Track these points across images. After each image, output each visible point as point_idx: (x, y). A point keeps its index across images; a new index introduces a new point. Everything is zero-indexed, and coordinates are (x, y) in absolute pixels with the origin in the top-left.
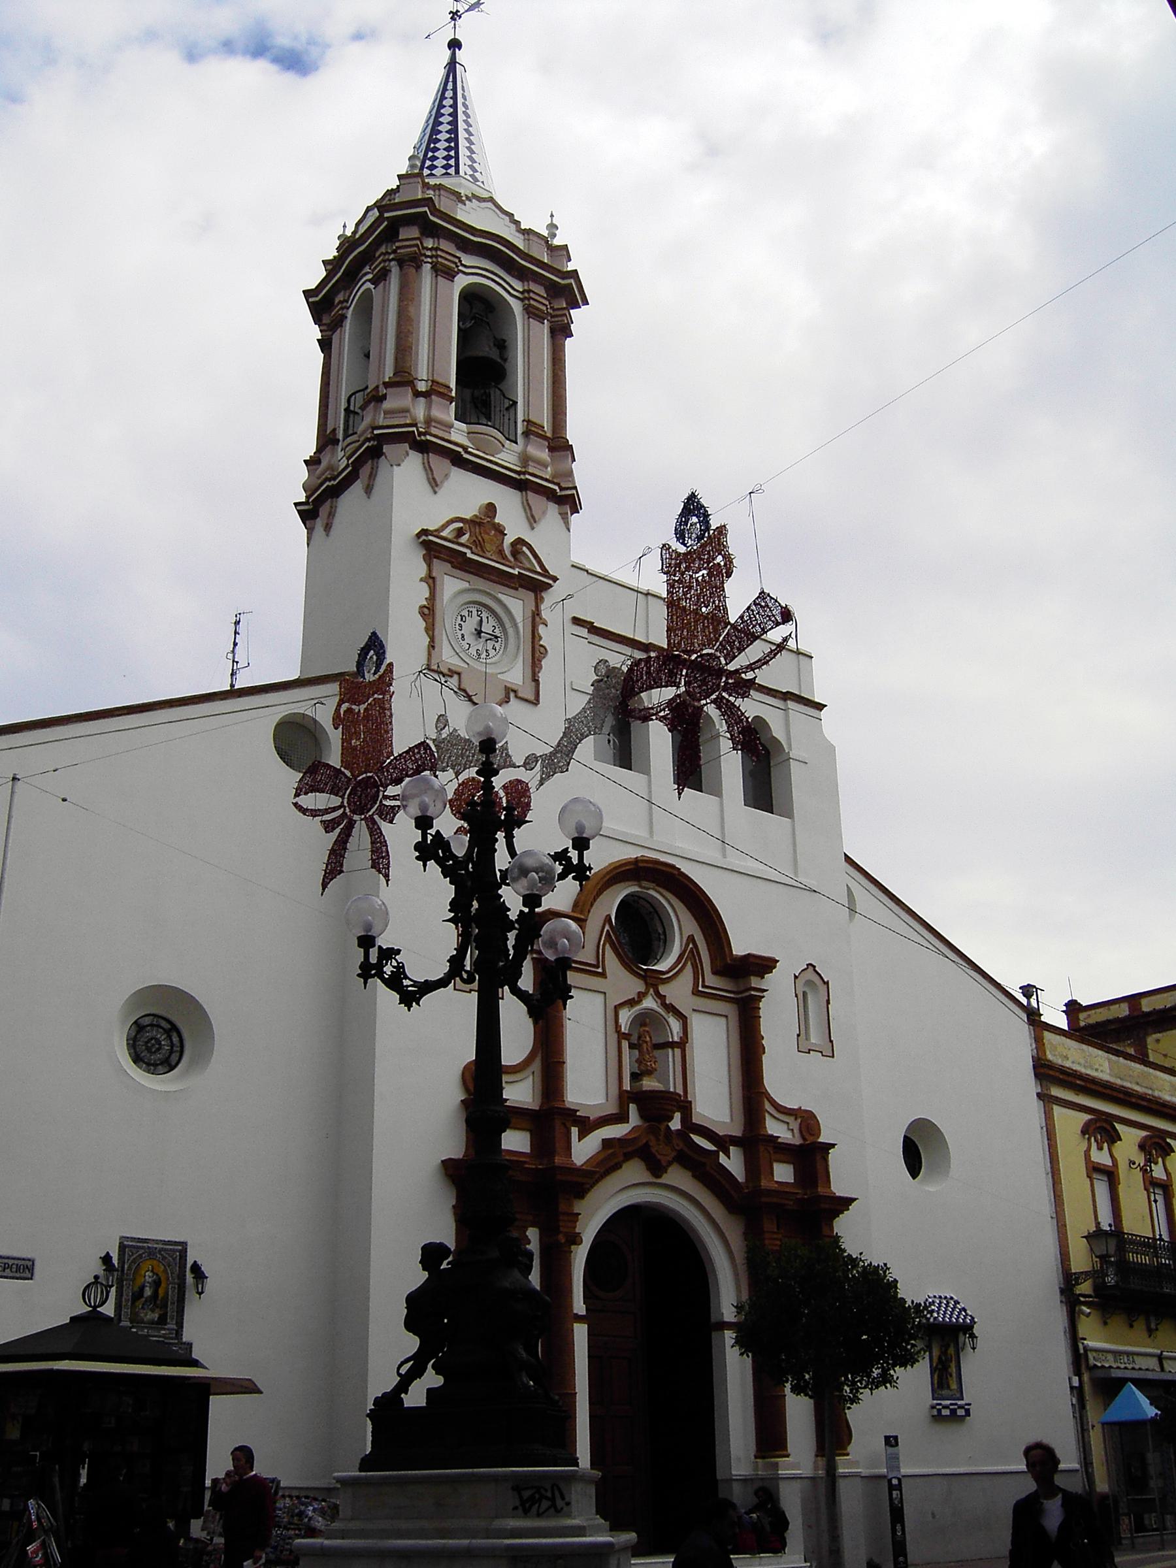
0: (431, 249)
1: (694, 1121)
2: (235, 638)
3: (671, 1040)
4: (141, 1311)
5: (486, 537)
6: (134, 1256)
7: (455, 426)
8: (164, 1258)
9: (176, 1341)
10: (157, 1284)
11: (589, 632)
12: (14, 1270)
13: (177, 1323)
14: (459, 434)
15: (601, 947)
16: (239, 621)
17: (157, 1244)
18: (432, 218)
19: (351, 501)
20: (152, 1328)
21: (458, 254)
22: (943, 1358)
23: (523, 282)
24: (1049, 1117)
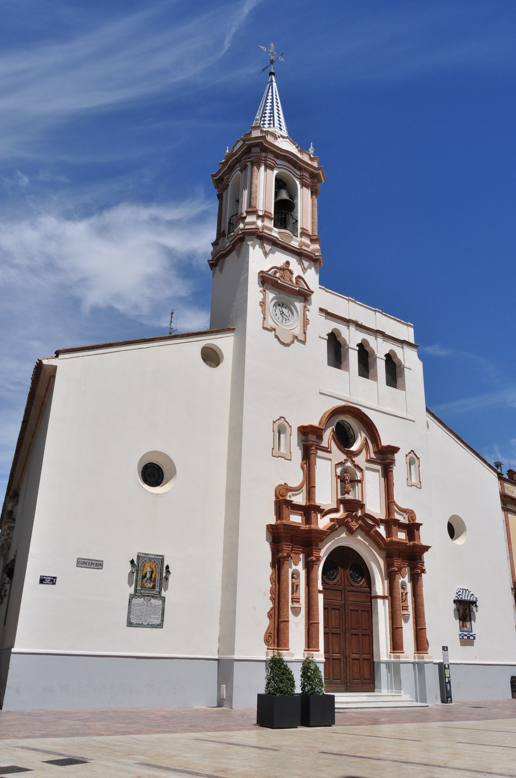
0: (264, 157)
1: (366, 512)
2: (171, 319)
3: (357, 479)
4: (146, 583)
5: (286, 275)
6: (143, 561)
7: (274, 230)
8: (155, 562)
9: (159, 596)
10: (152, 572)
12: (95, 565)
13: (159, 589)
14: (275, 233)
15: (330, 440)
16: (173, 313)
17: (152, 556)
18: (265, 144)
19: (231, 259)
20: (149, 590)
21: (275, 159)
22: (464, 615)
23: (300, 171)
24: (506, 518)
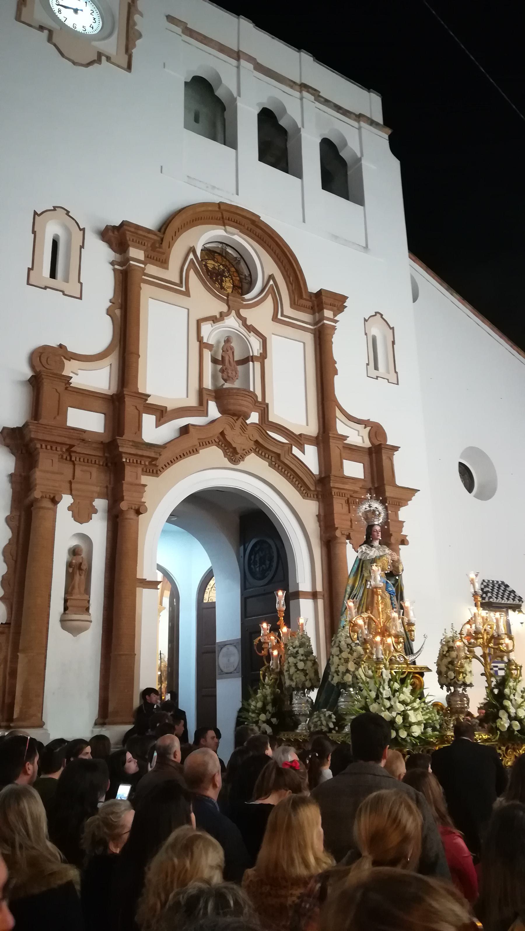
11: (183, 32)
